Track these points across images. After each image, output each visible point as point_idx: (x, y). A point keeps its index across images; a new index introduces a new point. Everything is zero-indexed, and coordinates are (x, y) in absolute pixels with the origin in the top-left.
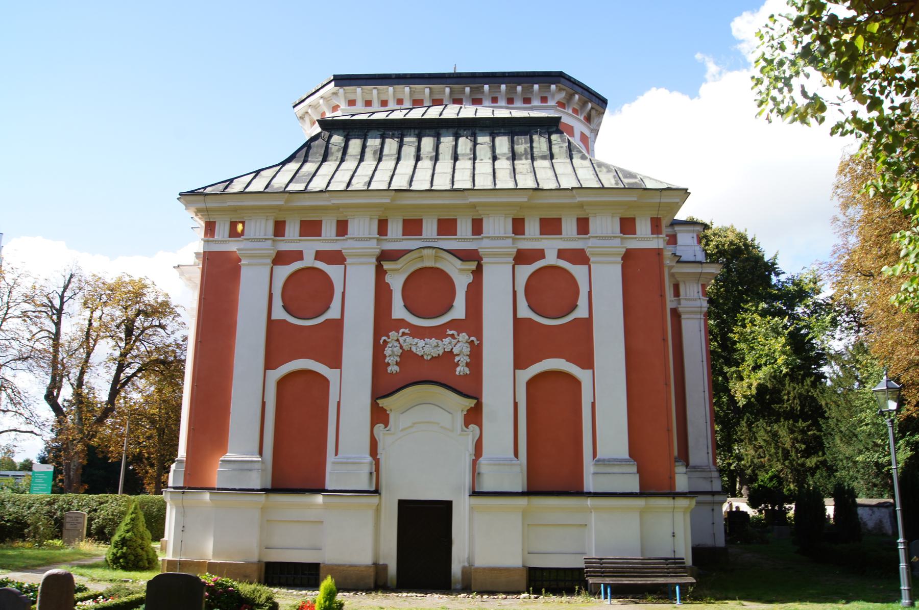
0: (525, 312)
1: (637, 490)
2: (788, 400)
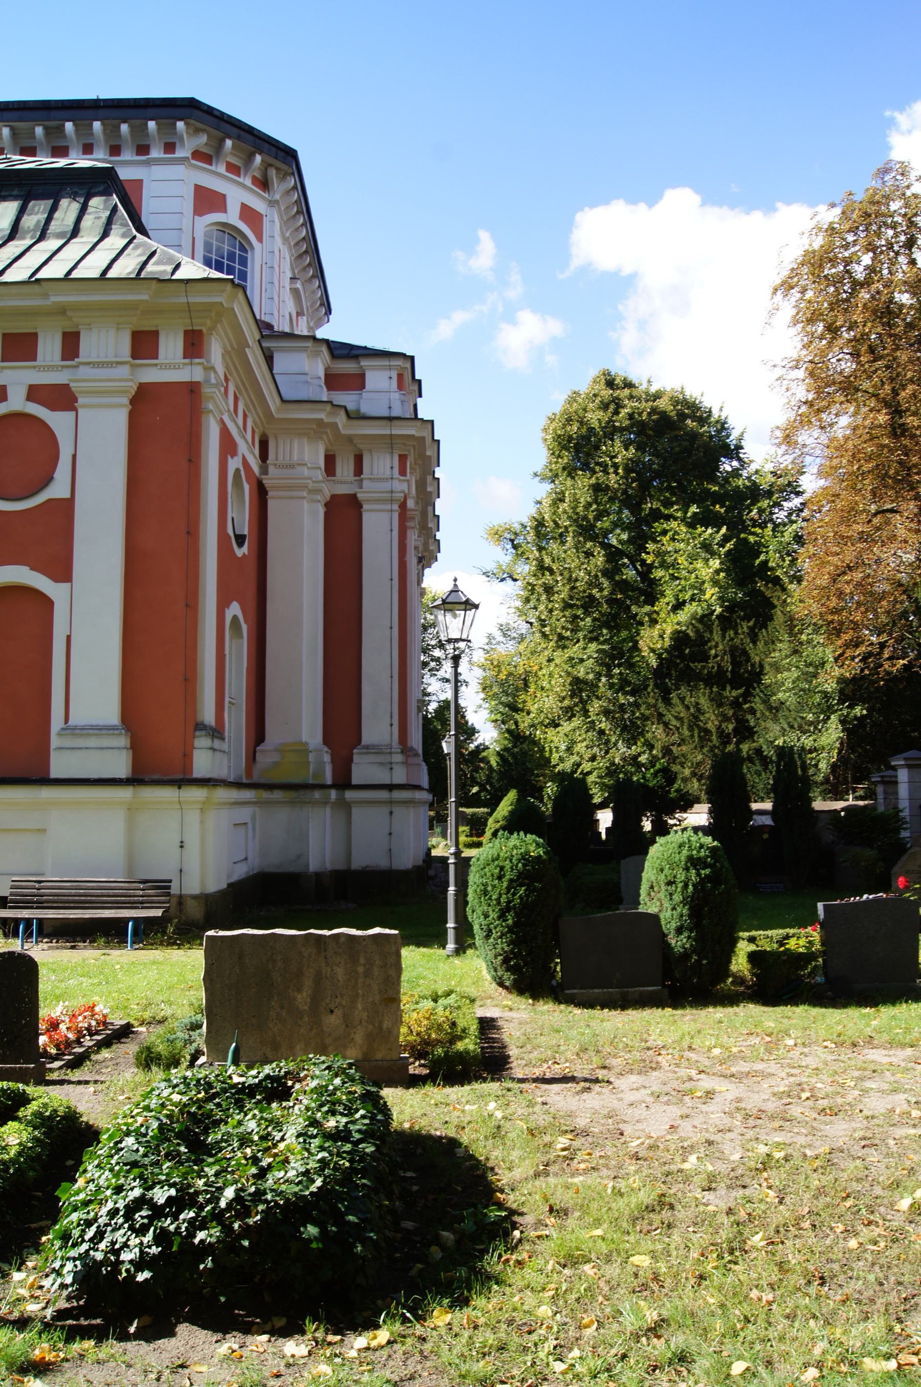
2: (716, 656)
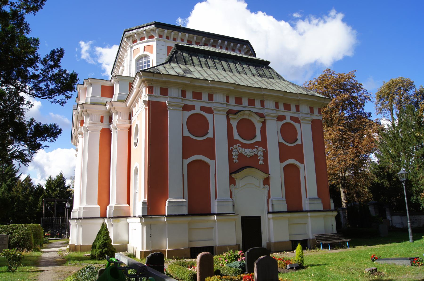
0: (187, 134)
1: (322, 209)
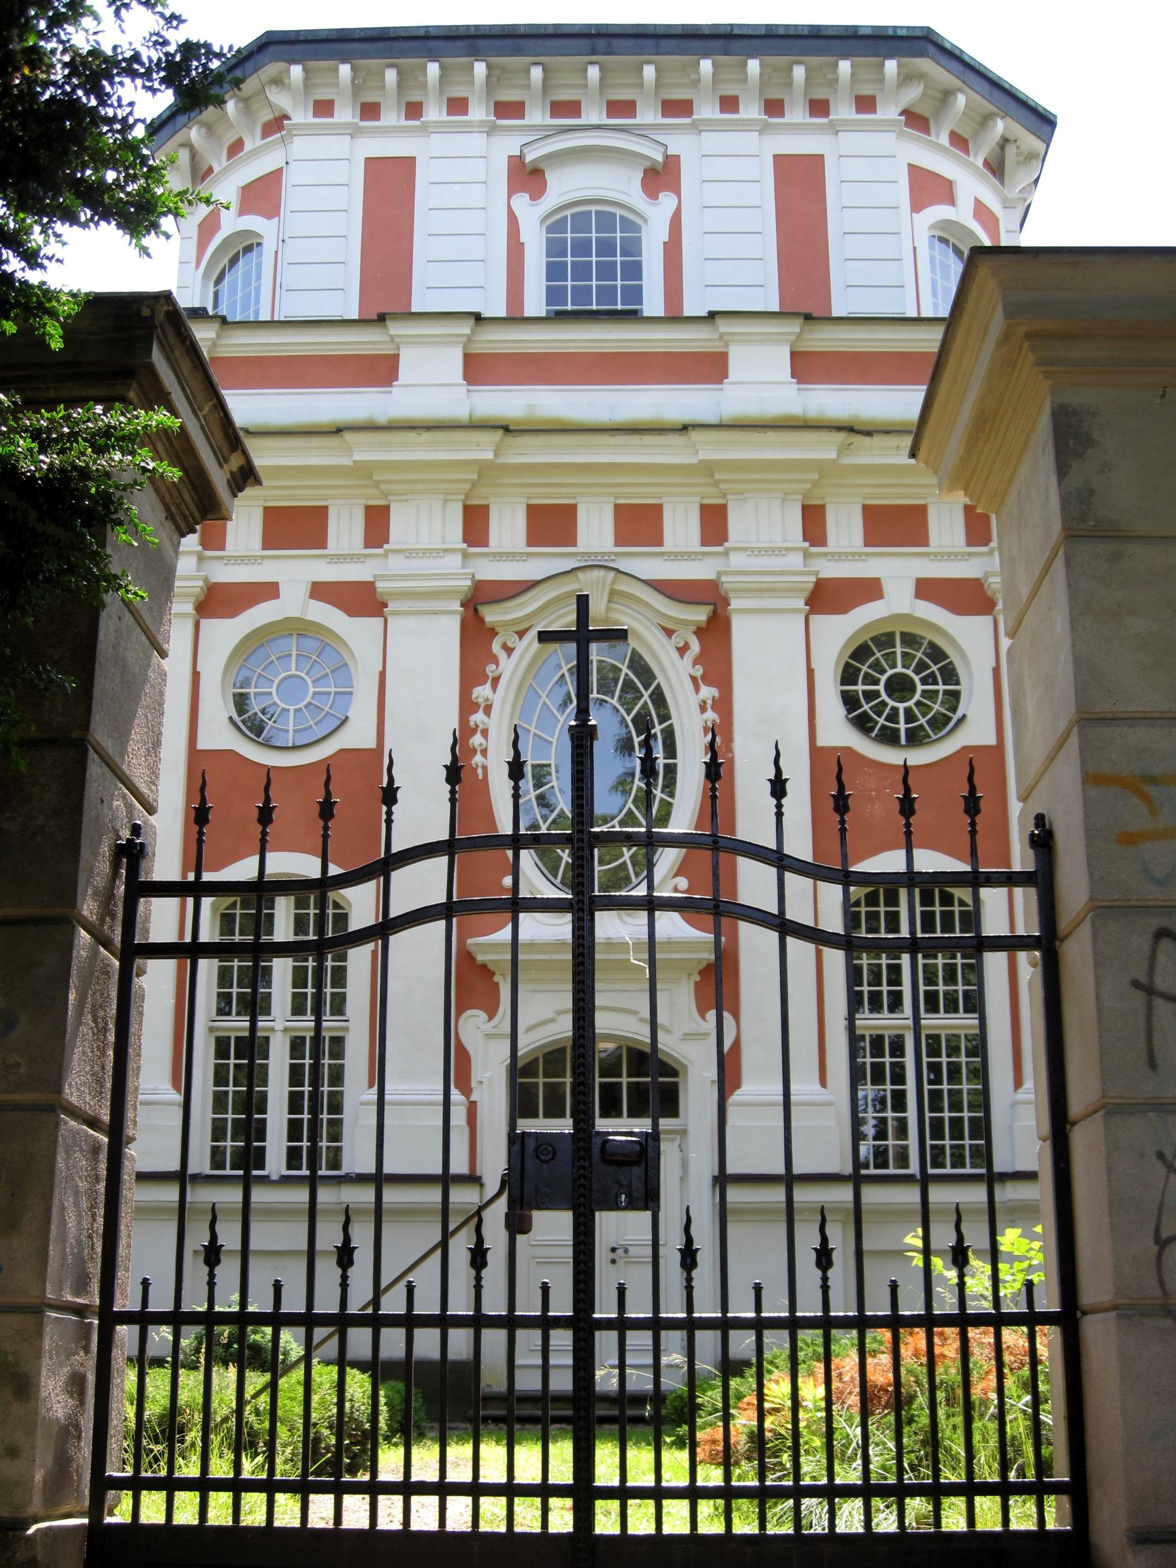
0: (837, 731)
